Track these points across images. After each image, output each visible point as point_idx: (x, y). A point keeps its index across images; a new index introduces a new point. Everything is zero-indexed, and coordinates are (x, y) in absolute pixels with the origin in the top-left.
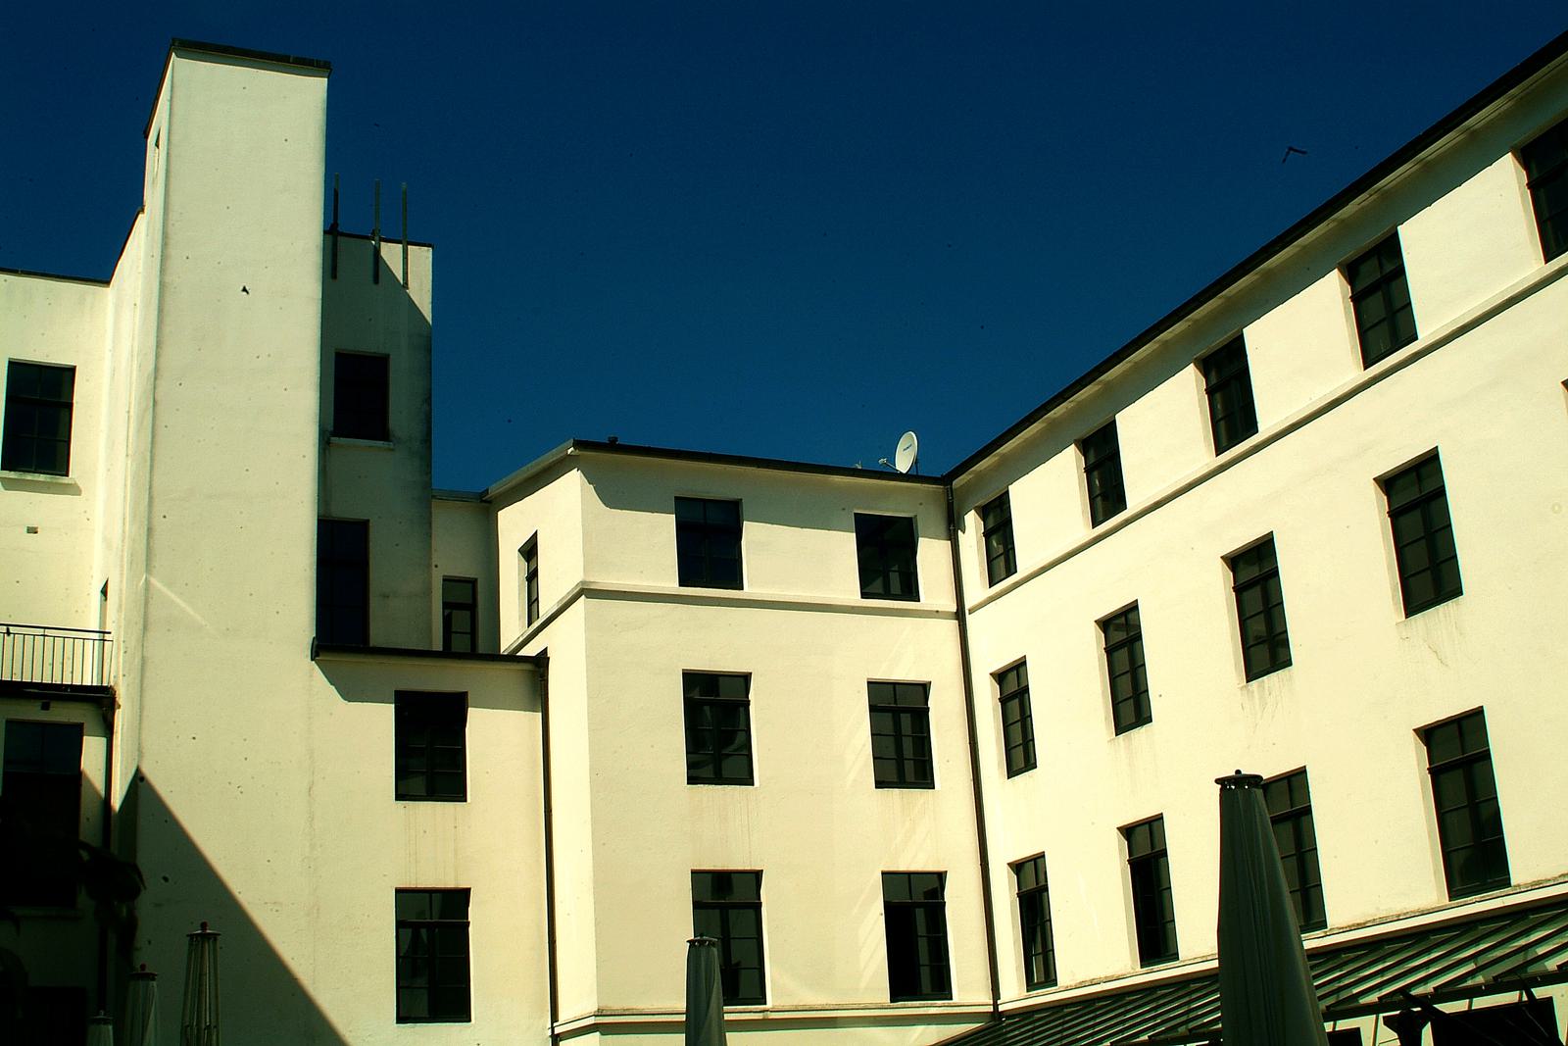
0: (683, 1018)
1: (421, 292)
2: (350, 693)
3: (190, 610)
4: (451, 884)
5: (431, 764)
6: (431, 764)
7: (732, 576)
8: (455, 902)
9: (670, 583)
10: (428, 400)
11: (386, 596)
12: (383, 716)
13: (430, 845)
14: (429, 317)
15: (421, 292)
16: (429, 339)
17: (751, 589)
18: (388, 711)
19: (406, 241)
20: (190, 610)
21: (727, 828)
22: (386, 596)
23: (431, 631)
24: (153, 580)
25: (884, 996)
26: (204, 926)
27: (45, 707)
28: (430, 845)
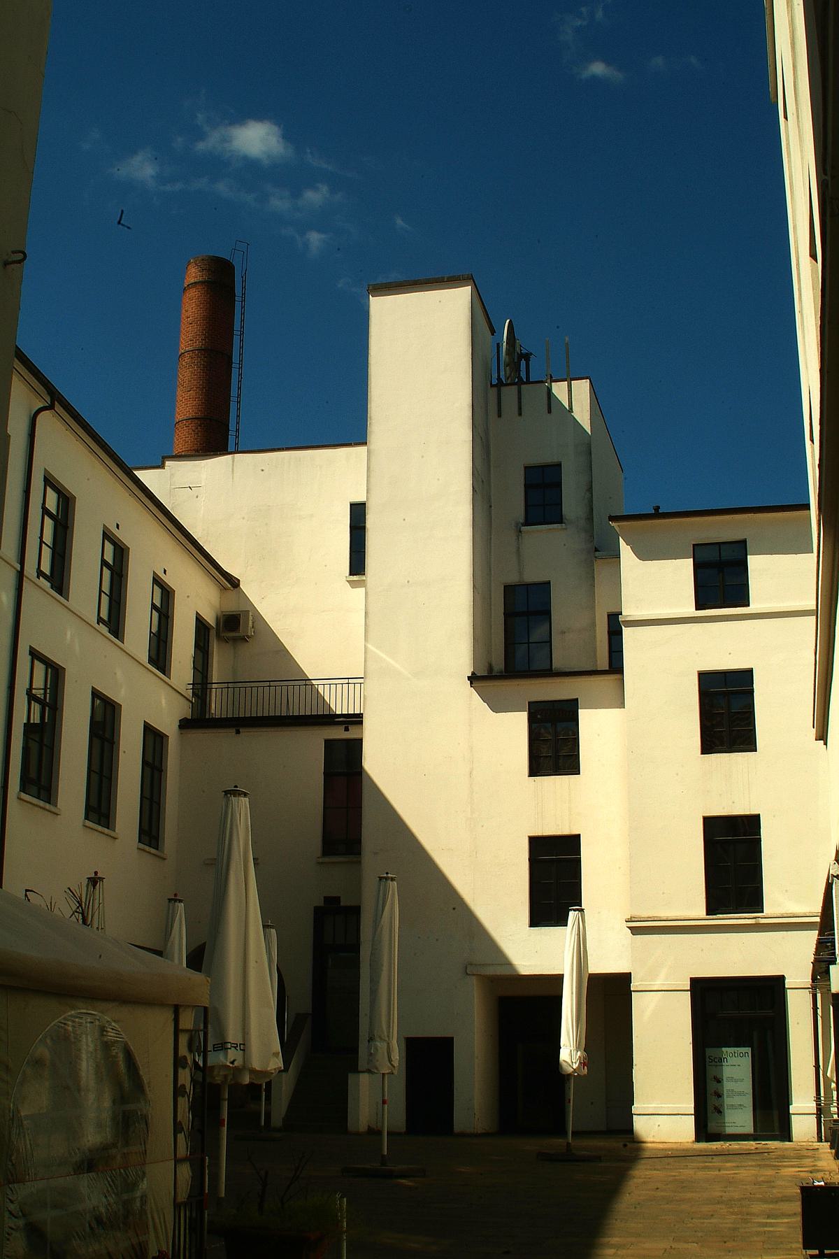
0: (818, 919)
1: (582, 414)
2: (496, 708)
3: (392, 662)
4: (566, 832)
5: (554, 749)
6: (554, 749)
7: (741, 597)
8: (571, 844)
9: (689, 609)
10: (590, 489)
11: (563, 633)
12: (519, 721)
13: (556, 805)
14: (588, 428)
15: (582, 414)
16: (589, 446)
17: (755, 606)
18: (523, 717)
19: (569, 379)
20: (392, 662)
21: (733, 785)
22: (563, 633)
23: (595, 652)
24: (369, 646)
25: (702, 912)
26: (96, 873)
27: (347, 729)
28: (556, 805)
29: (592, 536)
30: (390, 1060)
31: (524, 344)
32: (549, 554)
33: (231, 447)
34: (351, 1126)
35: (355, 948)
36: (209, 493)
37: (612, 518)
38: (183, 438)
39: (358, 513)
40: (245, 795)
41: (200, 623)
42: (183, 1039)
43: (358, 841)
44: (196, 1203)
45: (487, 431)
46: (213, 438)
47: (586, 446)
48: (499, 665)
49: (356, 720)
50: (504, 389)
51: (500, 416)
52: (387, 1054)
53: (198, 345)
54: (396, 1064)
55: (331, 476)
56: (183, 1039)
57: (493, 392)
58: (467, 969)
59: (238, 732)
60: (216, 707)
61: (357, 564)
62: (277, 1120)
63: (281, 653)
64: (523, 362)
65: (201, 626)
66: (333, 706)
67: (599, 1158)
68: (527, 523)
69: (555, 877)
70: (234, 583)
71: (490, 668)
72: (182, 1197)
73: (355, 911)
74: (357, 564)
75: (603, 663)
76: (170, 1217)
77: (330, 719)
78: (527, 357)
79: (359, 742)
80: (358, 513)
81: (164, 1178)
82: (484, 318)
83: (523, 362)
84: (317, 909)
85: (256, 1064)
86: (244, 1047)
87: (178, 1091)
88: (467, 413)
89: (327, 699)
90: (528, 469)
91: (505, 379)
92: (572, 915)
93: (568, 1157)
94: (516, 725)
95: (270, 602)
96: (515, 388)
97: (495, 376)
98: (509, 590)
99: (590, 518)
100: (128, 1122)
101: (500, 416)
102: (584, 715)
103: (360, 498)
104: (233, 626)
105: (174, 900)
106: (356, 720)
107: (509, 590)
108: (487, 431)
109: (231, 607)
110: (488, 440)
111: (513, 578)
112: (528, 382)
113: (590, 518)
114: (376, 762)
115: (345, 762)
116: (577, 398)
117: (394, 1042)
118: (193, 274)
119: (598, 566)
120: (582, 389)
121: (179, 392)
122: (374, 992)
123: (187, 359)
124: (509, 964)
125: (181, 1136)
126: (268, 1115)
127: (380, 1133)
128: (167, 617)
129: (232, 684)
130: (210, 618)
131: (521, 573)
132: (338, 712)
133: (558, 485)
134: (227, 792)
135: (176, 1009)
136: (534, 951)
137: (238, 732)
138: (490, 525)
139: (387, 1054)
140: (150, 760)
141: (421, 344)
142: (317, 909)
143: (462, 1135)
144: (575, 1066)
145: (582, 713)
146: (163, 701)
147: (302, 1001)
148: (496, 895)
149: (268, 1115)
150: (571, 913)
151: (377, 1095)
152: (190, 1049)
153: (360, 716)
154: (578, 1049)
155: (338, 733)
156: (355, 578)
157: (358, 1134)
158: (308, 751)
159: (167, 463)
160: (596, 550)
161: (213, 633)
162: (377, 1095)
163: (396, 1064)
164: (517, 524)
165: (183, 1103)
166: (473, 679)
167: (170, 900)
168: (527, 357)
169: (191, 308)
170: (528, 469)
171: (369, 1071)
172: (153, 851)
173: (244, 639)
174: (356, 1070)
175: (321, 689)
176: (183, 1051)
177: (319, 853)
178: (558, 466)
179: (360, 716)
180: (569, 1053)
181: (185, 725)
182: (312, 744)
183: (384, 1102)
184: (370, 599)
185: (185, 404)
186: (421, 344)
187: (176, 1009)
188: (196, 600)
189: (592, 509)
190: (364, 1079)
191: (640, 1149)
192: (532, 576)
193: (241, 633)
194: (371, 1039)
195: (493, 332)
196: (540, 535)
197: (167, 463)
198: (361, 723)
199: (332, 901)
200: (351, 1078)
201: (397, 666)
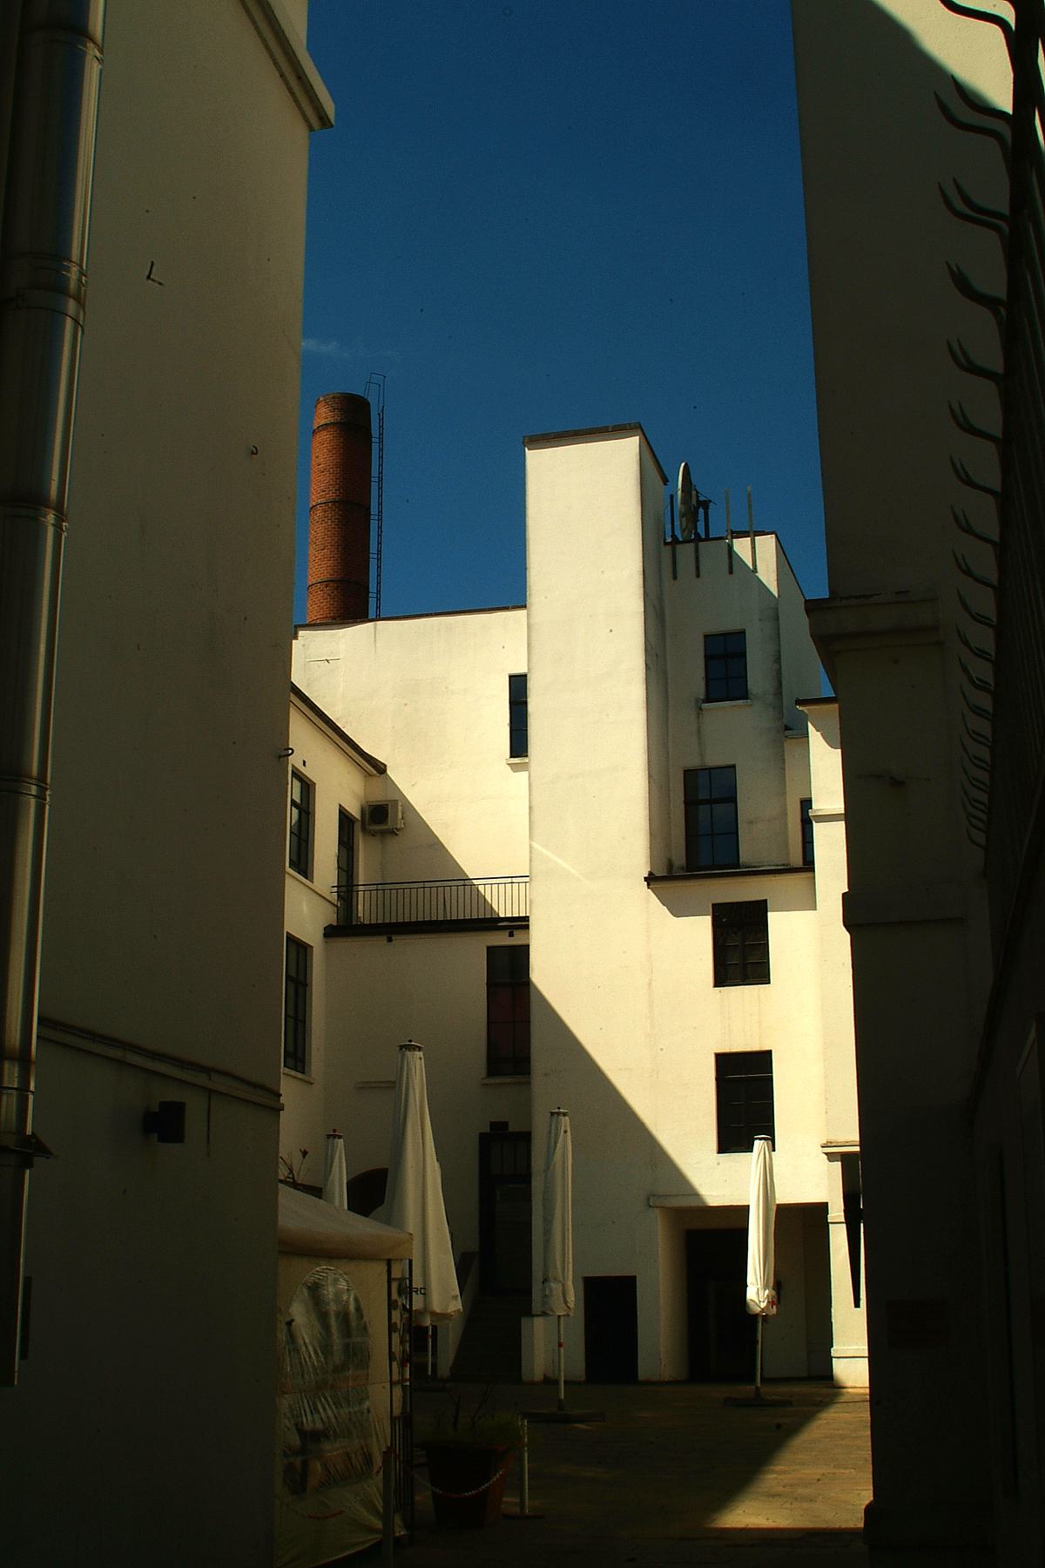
1: (768, 574)
2: (677, 911)
3: (560, 861)
5: (741, 955)
6: (741, 955)
8: (762, 1061)
10: (778, 660)
11: (751, 822)
15: (768, 574)
18: (707, 921)
19: (752, 533)
22: (751, 822)
23: (787, 845)
27: (511, 935)
28: (742, 1019)
29: (781, 713)
30: (566, 1302)
31: (704, 490)
32: (733, 733)
33: (372, 614)
34: (525, 1376)
35: (526, 1178)
36: (346, 669)
37: (799, 702)
38: (315, 604)
39: (518, 687)
40: (420, 1049)
41: (344, 816)
42: (395, 1286)
43: (526, 1060)
44: (404, 1422)
45: (660, 599)
46: (352, 604)
47: (772, 611)
48: (680, 858)
49: (522, 923)
50: (679, 547)
51: (675, 578)
52: (564, 1295)
53: (331, 496)
54: (572, 1305)
55: (484, 646)
56: (395, 1286)
57: (667, 551)
58: (651, 1201)
59: (390, 940)
60: (364, 910)
61: (519, 745)
62: (444, 1369)
63: (435, 847)
64: (701, 511)
65: (345, 818)
66: (495, 907)
67: (790, 1403)
68: (708, 700)
69: (745, 1098)
70: (380, 768)
71: (670, 865)
72: (397, 1412)
73: (526, 1137)
74: (519, 745)
75: (796, 859)
76: (388, 1430)
77: (492, 923)
78: (705, 505)
79: (524, 951)
80: (518, 687)
81: (382, 1395)
82: (654, 469)
83: (701, 511)
84: (482, 1136)
85: (437, 1308)
86: (425, 1292)
87: (392, 1328)
88: (637, 581)
89: (488, 898)
90: (708, 638)
91: (680, 535)
92: (758, 1145)
93: (758, 1402)
94: (700, 929)
95: (420, 787)
96: (690, 547)
97: (669, 532)
98: (690, 776)
99: (779, 693)
100: (357, 1355)
101: (675, 578)
102: (774, 919)
103: (521, 669)
104: (381, 818)
105: (334, 1136)
106: (522, 923)
107: (690, 776)
108: (660, 599)
109: (378, 796)
110: (662, 607)
111: (693, 762)
112: (708, 539)
113: (779, 693)
114: (545, 973)
115: (509, 969)
116: (761, 556)
117: (570, 1283)
118: (324, 415)
119: (788, 745)
120: (767, 544)
121: (312, 550)
122: (548, 1232)
123: (319, 513)
124: (697, 1195)
125: (394, 1364)
126: (434, 1366)
127: (556, 1382)
128: (308, 813)
129: (380, 886)
130: (354, 810)
131: (702, 756)
132: (502, 915)
133: (742, 655)
134: (401, 1047)
135: (389, 1262)
136: (723, 1180)
137: (390, 940)
138: (666, 685)
139: (564, 1295)
140: (293, 974)
141: (585, 503)
142: (482, 1136)
143: (648, 1383)
144: (763, 1305)
145: (772, 917)
146: (305, 908)
147: (473, 1244)
148: (682, 1122)
149: (434, 1366)
150: (757, 1143)
151: (552, 1341)
152: (400, 1294)
153: (526, 919)
154: (766, 1287)
155: (501, 939)
156: (516, 760)
157: (533, 1384)
158: (467, 961)
159: (301, 633)
160: (787, 728)
161: (358, 827)
162: (552, 1341)
163: (572, 1305)
164: (697, 701)
165: (396, 1337)
166: (650, 880)
167: (329, 1136)
168: (705, 505)
169: (321, 454)
170: (708, 638)
171: (544, 1314)
172: (299, 1075)
173: (393, 833)
174: (530, 1314)
175: (481, 888)
176: (395, 1296)
177: (484, 1074)
178: (742, 633)
179: (526, 919)
180: (757, 1292)
181: (330, 932)
182: (471, 954)
183: (560, 1345)
184: (534, 659)
185: (316, 562)
186: (585, 503)
187: (389, 1262)
188: (338, 791)
189: (780, 682)
190: (539, 1323)
191: (838, 1394)
192: (715, 759)
193: (390, 825)
194: (545, 1280)
195: (665, 481)
196: (726, 714)
197: (301, 633)
198: (527, 927)
199: (499, 1128)
200: (524, 1320)
201: (565, 865)
